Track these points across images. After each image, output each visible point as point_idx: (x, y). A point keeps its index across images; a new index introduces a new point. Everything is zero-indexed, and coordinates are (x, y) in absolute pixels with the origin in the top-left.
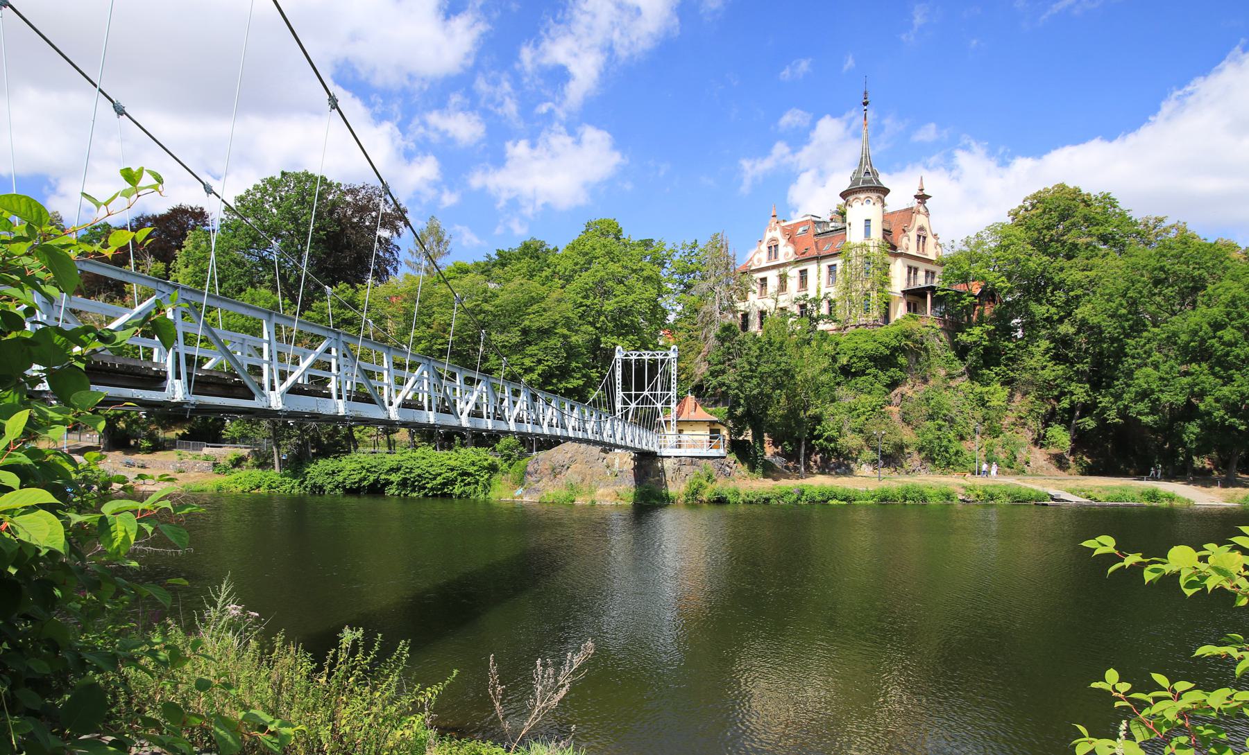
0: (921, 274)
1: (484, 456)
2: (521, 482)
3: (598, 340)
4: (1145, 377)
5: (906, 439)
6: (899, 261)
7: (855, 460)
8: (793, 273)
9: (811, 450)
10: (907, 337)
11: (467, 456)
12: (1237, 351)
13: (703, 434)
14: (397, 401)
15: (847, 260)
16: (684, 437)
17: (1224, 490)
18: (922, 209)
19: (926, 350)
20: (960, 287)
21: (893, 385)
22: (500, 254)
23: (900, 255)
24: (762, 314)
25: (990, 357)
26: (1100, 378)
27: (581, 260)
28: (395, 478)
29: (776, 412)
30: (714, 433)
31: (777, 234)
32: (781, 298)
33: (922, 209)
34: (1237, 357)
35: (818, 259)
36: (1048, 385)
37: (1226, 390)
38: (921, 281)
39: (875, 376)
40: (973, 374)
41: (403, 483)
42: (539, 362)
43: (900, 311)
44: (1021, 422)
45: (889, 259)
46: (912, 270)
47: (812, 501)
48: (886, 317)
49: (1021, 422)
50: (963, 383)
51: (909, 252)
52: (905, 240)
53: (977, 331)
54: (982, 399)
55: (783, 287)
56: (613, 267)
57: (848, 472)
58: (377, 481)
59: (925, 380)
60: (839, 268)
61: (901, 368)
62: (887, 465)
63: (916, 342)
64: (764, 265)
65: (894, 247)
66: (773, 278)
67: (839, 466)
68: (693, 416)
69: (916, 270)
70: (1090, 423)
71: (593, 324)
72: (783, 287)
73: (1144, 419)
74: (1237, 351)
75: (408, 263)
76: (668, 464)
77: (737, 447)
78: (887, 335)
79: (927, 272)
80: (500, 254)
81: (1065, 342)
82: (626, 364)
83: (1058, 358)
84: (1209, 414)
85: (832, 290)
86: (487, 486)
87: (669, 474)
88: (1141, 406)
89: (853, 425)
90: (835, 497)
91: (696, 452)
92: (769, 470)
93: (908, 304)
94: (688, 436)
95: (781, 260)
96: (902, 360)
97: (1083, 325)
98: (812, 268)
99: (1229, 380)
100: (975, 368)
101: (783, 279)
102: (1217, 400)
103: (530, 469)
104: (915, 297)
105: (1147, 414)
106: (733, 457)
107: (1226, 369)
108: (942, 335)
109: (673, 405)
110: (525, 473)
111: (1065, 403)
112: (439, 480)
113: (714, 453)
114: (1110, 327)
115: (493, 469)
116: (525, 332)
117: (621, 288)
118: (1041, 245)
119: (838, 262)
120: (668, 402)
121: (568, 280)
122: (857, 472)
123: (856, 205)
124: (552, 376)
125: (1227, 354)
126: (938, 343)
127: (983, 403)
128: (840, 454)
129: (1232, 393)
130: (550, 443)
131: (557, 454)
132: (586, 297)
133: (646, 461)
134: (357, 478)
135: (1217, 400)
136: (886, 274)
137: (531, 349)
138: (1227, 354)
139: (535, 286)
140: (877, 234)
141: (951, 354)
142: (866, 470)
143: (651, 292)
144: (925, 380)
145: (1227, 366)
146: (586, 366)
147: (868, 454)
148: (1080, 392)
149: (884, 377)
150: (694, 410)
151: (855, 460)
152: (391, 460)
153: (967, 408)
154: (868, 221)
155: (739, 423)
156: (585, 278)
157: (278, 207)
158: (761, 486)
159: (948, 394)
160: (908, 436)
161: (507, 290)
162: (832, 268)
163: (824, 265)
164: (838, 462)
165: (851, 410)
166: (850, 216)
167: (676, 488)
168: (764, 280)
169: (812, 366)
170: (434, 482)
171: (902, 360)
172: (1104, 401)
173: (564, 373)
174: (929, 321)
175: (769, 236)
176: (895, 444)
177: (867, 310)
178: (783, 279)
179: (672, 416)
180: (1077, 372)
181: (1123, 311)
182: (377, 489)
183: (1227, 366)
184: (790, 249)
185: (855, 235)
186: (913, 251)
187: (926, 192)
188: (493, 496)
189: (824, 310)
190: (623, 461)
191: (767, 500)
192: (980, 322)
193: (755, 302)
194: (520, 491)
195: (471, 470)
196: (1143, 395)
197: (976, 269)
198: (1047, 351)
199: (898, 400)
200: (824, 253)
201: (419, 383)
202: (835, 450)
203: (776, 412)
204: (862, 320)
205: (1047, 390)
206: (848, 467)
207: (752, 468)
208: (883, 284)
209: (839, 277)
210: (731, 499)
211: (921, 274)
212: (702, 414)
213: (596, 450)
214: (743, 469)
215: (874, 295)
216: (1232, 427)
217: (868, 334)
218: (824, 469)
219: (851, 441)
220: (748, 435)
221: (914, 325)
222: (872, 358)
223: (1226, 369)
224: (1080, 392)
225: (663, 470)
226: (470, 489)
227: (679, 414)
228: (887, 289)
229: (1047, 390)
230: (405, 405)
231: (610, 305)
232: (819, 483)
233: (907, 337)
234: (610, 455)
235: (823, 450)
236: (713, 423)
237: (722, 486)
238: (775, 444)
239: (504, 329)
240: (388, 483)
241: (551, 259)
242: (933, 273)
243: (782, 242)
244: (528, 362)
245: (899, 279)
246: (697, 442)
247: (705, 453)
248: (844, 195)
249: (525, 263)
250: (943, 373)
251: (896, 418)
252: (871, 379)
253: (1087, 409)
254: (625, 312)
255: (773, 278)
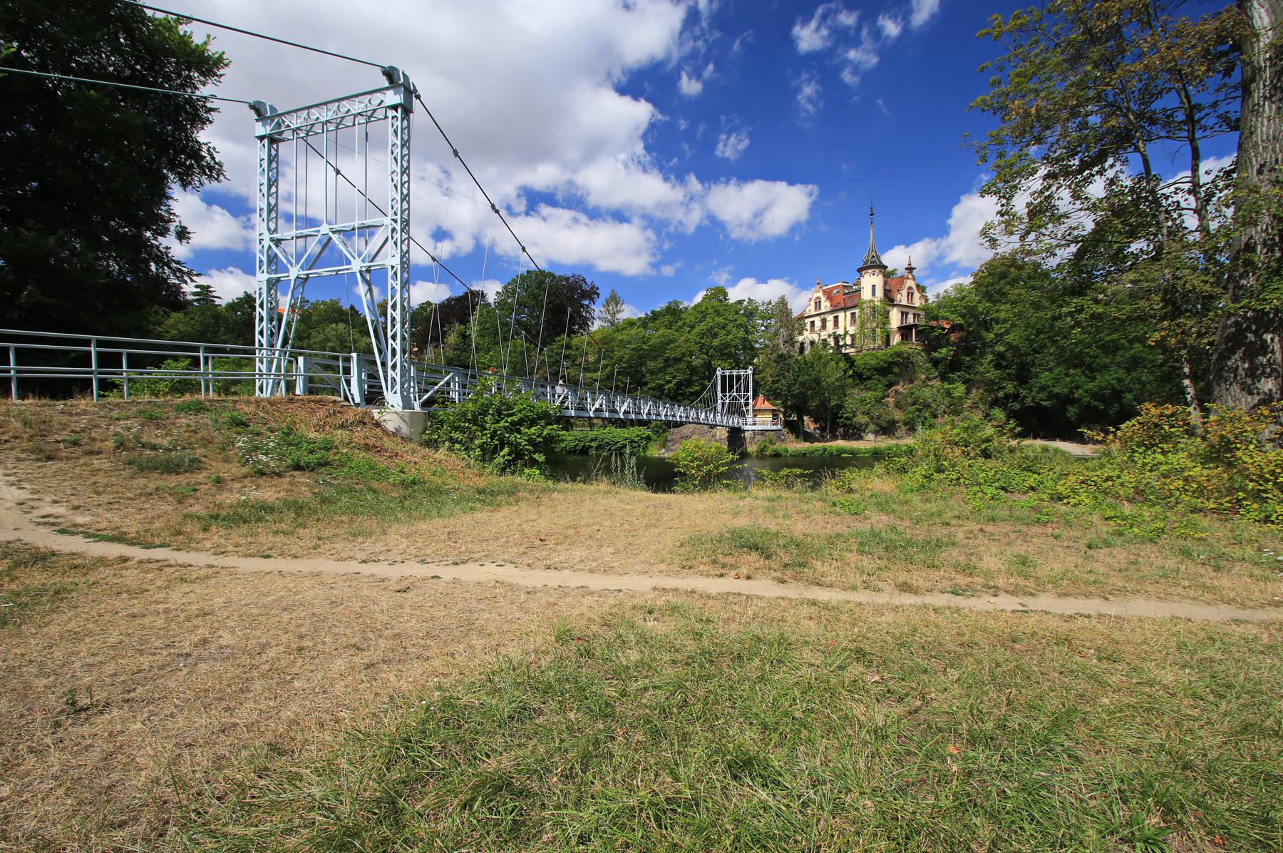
0: (911, 316)
1: (645, 432)
2: (664, 446)
3: (710, 362)
4: (1045, 378)
5: (897, 418)
6: (895, 309)
7: (864, 431)
8: (830, 318)
9: (838, 425)
10: (899, 356)
11: (634, 432)
12: (1098, 361)
13: (769, 417)
14: (593, 409)
15: (862, 310)
16: (756, 419)
17: (1093, 446)
18: (910, 276)
19: (912, 363)
20: (934, 323)
21: (890, 385)
22: (653, 312)
23: (896, 305)
24: (812, 343)
25: (954, 365)
26: (1023, 376)
27: (700, 316)
28: (593, 444)
29: (813, 404)
30: (775, 416)
31: (820, 294)
32: (822, 333)
33: (910, 276)
34: (1098, 364)
35: (845, 309)
36: (992, 382)
37: (1090, 385)
38: (910, 320)
39: (879, 380)
40: (943, 378)
41: (599, 447)
42: (674, 377)
43: (896, 339)
44: (975, 406)
45: (888, 308)
46: (904, 315)
47: (831, 454)
48: (888, 343)
49: (975, 406)
50: (937, 383)
51: (902, 303)
52: (899, 296)
53: (944, 351)
54: (949, 392)
55: (824, 327)
56: (718, 319)
57: (860, 438)
58: (584, 446)
59: (911, 382)
60: (857, 315)
61: (895, 375)
62: (884, 433)
63: (904, 358)
64: (813, 313)
65: (892, 300)
66: (818, 322)
67: (854, 434)
68: (763, 407)
69: (907, 314)
70: (1017, 406)
71: (707, 353)
72: (824, 327)
73: (1044, 403)
74: (1098, 361)
75: (600, 318)
76: (747, 435)
77: (788, 424)
78: (884, 354)
79: (914, 315)
80: (653, 312)
81: (1001, 356)
82: (723, 377)
83: (998, 366)
84: (1080, 399)
85: (853, 328)
86: (645, 448)
87: (748, 440)
88: (1042, 395)
89: (863, 410)
90: (845, 452)
91: (764, 428)
92: (808, 437)
93: (902, 335)
94: (759, 418)
95: (823, 310)
96: (896, 370)
97: (1010, 346)
98: (841, 315)
99: (1093, 379)
100: (945, 373)
101: (824, 322)
102: (1086, 391)
103: (669, 438)
104: (905, 331)
105: (1046, 400)
106: (785, 431)
107: (1092, 372)
108: (923, 354)
109: (750, 401)
110: (666, 441)
111: (1001, 394)
112: (618, 445)
113: (774, 428)
114: (1024, 347)
115: (649, 438)
116: (667, 360)
117: (723, 332)
118: (988, 296)
119: (857, 311)
120: (748, 399)
121: (693, 327)
122: (866, 438)
123: (867, 276)
124: (682, 385)
125: (1092, 363)
126: (920, 359)
127: (949, 394)
128: (855, 428)
129: (1095, 387)
130: (681, 424)
131: (685, 430)
132: (702, 338)
133: (735, 435)
134: (573, 444)
135: (1086, 391)
136: (887, 317)
137: (670, 370)
138: (1092, 363)
139: (672, 333)
140: (880, 293)
141: (929, 365)
142: (871, 436)
143: (741, 333)
144: (911, 382)
145: (1092, 370)
146: (701, 378)
147: (872, 427)
148: (1010, 387)
149: (884, 381)
150: (762, 403)
151: (864, 431)
152: (592, 434)
153: (939, 398)
154: (874, 286)
155: (788, 409)
156: (702, 327)
157: (526, 291)
158: (803, 446)
159: (926, 390)
160: (898, 415)
161: (656, 335)
162: (853, 314)
163: (848, 313)
164: (854, 432)
165: (862, 401)
166: (863, 284)
167: (752, 448)
168: (813, 323)
169: (833, 374)
170: (161, 483)
171: (896, 370)
172: (1023, 392)
173: (689, 383)
174: (914, 346)
175: (815, 295)
176: (889, 421)
177: (874, 340)
178: (824, 322)
179: (750, 407)
180: (1008, 374)
181: (1033, 337)
182: (585, 451)
183: (1092, 370)
184: (828, 304)
185: (866, 295)
186: (904, 302)
187: (913, 266)
188: (649, 453)
189: (848, 340)
190: (722, 433)
191: (805, 454)
192: (948, 344)
193: (807, 336)
194: (663, 451)
195: (636, 439)
196: (1042, 389)
197: (943, 313)
198: (991, 361)
199: (893, 394)
200: (848, 305)
201: (601, 401)
202: (851, 425)
203: (813, 404)
204: (872, 346)
205: (991, 386)
206: (860, 435)
207: (797, 437)
208: (884, 324)
209: (858, 320)
210: (784, 454)
211: (911, 316)
212: (767, 405)
213: (706, 427)
214: (792, 437)
215: (878, 331)
216: (1096, 408)
217: (873, 355)
218: (845, 437)
219: (861, 419)
220: (794, 418)
221: (904, 348)
222: (875, 369)
223: (1092, 372)
224: (1010, 387)
225: (744, 438)
226: (636, 450)
227: (754, 406)
228: (887, 326)
229: (991, 386)
230: (597, 410)
231: (716, 343)
232: (840, 443)
233: (899, 356)
234: (714, 430)
235: (845, 425)
236: (773, 410)
237: (779, 446)
238: (815, 422)
239: (655, 359)
240: (590, 447)
241: (683, 316)
242: (919, 315)
243: (823, 299)
244: (668, 378)
245: (895, 319)
246: (764, 422)
247: (769, 427)
248: (860, 270)
249: (667, 319)
250: (924, 377)
251: (891, 405)
252: (876, 382)
253: (1016, 397)
254: (727, 345)
255: (818, 322)
